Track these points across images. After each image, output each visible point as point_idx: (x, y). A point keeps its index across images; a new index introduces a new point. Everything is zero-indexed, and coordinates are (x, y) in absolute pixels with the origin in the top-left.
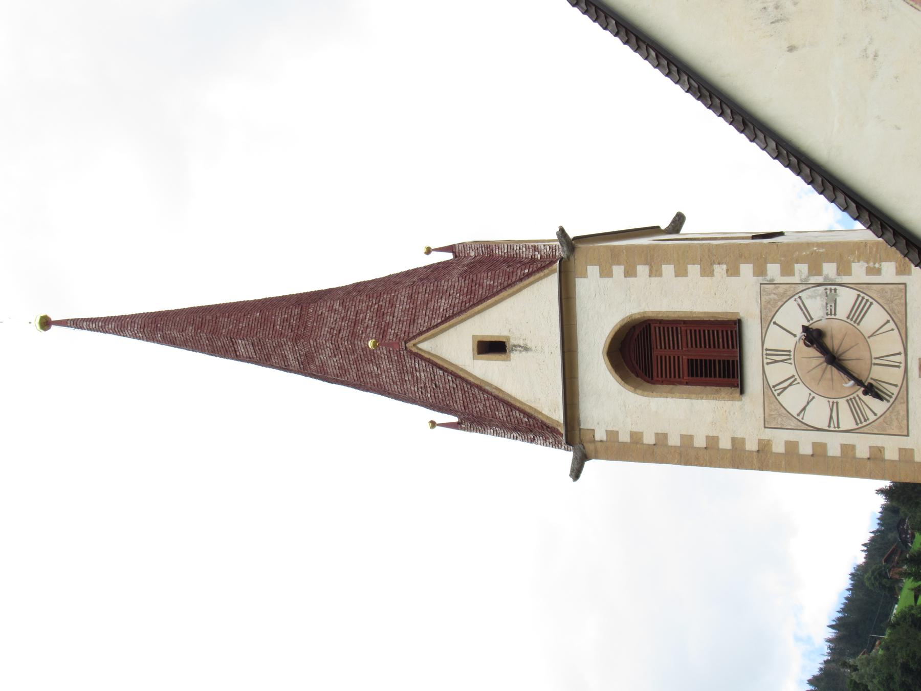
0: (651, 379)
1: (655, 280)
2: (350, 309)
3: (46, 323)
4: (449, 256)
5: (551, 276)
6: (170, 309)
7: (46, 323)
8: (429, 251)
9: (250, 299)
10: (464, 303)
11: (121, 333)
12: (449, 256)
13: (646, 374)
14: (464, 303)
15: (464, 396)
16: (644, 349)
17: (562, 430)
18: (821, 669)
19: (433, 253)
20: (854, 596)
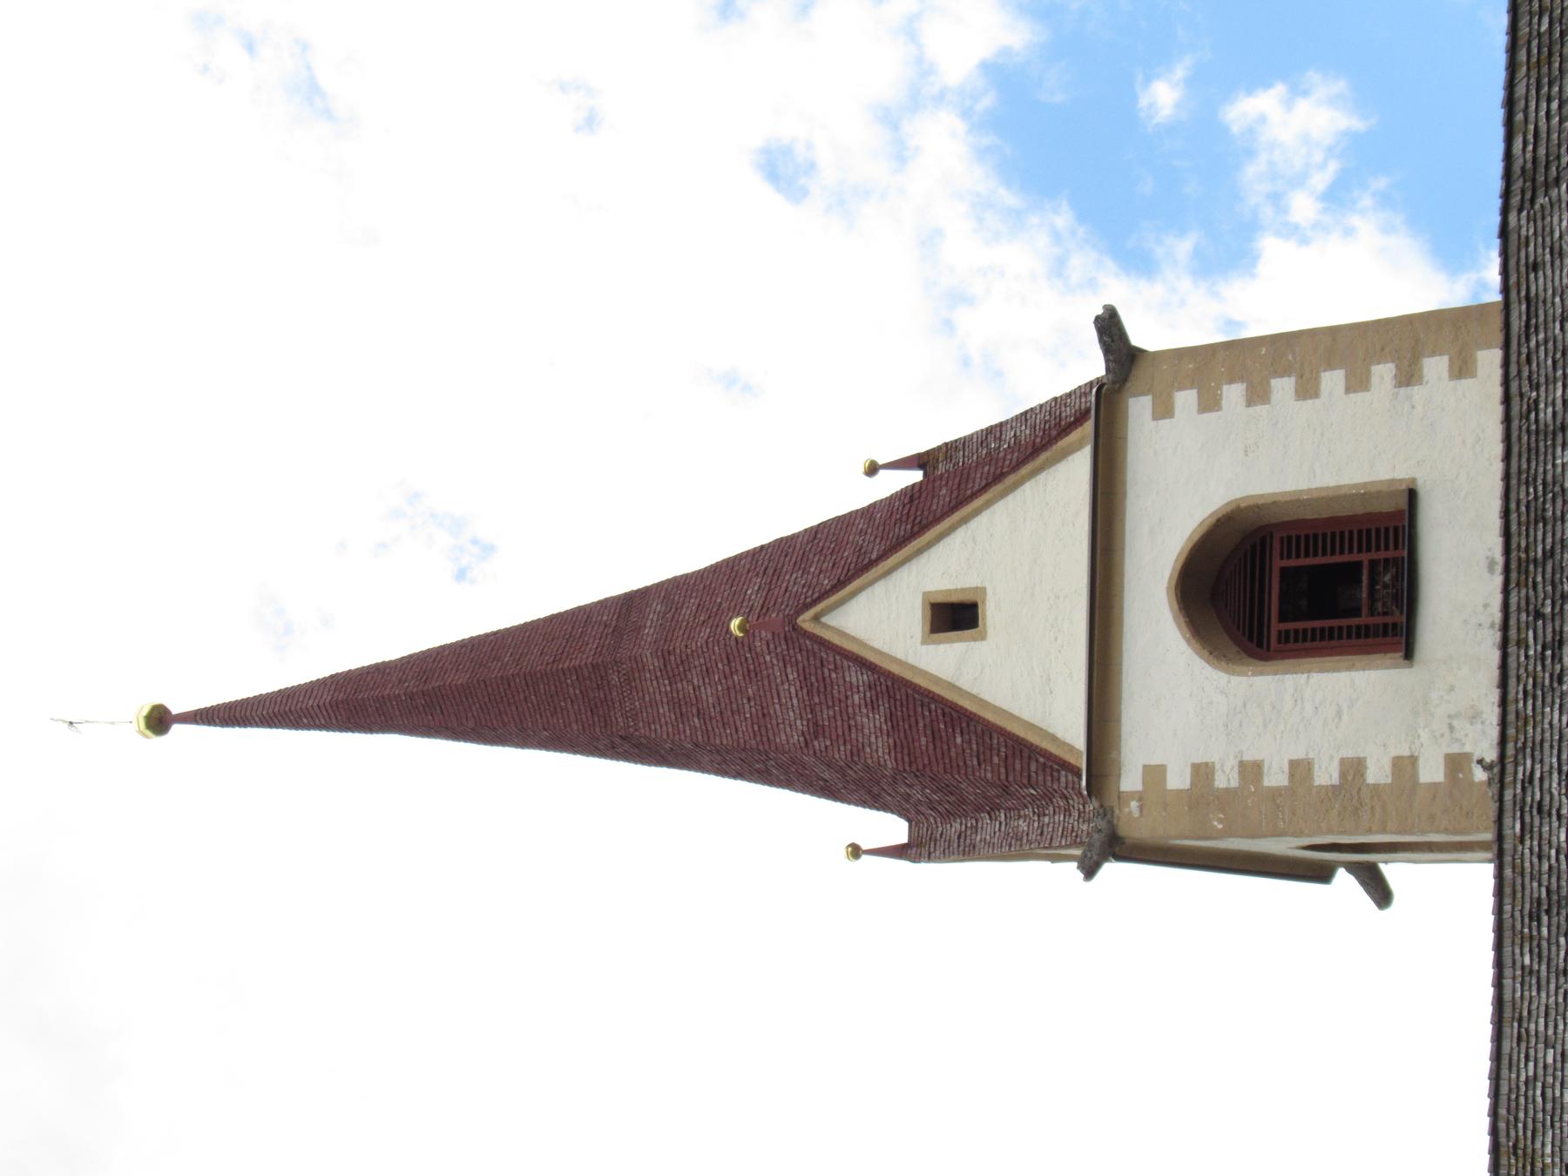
0: (1241, 632)
1: (1260, 410)
2: (819, 549)
3: (159, 721)
4: (916, 476)
5: (1046, 472)
6: (664, 579)
7: (159, 721)
8: (872, 469)
9: (689, 570)
10: (465, 670)
11: (247, 722)
12: (916, 476)
13: (1239, 628)
14: (465, 670)
15: (874, 747)
16: (1252, 599)
17: (1083, 765)
19: (882, 473)
20: (1461, 776)
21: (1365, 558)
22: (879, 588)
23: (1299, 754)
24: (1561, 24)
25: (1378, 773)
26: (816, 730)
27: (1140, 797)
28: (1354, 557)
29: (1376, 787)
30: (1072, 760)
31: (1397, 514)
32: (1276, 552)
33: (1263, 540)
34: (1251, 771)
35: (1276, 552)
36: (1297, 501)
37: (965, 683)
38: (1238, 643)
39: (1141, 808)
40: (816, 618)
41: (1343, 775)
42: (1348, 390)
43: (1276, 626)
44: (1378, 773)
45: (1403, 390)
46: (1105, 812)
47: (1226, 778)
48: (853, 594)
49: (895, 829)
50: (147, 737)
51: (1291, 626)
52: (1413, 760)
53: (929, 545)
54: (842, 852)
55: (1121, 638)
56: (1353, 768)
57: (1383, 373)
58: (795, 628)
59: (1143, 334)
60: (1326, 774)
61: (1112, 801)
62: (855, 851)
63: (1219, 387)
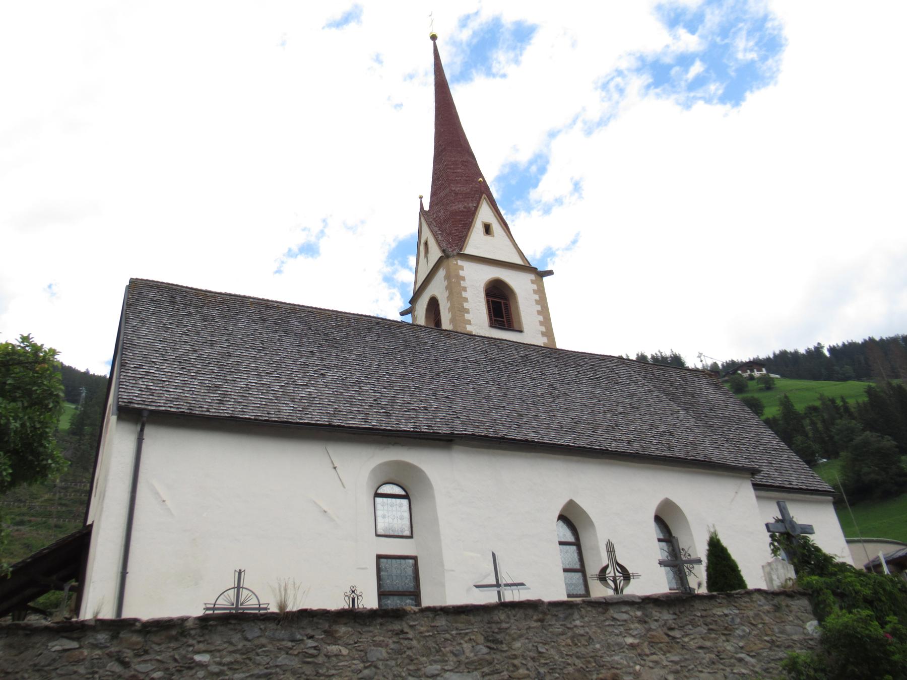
3: (434, 38)
7: (434, 38)
18: (865, 341)
21: (505, 320)
22: (492, 214)
23: (469, 300)
24: (283, 640)
25: (467, 316)
26: (456, 194)
27: (457, 264)
28: (505, 318)
29: (464, 316)
30: (463, 250)
31: (513, 327)
32: (505, 302)
33: (506, 299)
34: (465, 289)
35: (505, 302)
36: (517, 308)
37: (475, 229)
38: (488, 288)
39: (455, 264)
40: (485, 198)
41: (466, 309)
42: (540, 321)
43: (490, 299)
44: (467, 316)
45: (540, 332)
46: (454, 256)
47: (463, 284)
48: (490, 207)
49: (426, 208)
50: (431, 34)
51: (491, 302)
52: (471, 324)
53: (501, 226)
54: (421, 194)
55: (487, 265)
56: (467, 311)
57: (543, 329)
58: (483, 193)
59: (546, 279)
60: (466, 305)
61: (456, 258)
62: (421, 198)
63: (538, 294)
